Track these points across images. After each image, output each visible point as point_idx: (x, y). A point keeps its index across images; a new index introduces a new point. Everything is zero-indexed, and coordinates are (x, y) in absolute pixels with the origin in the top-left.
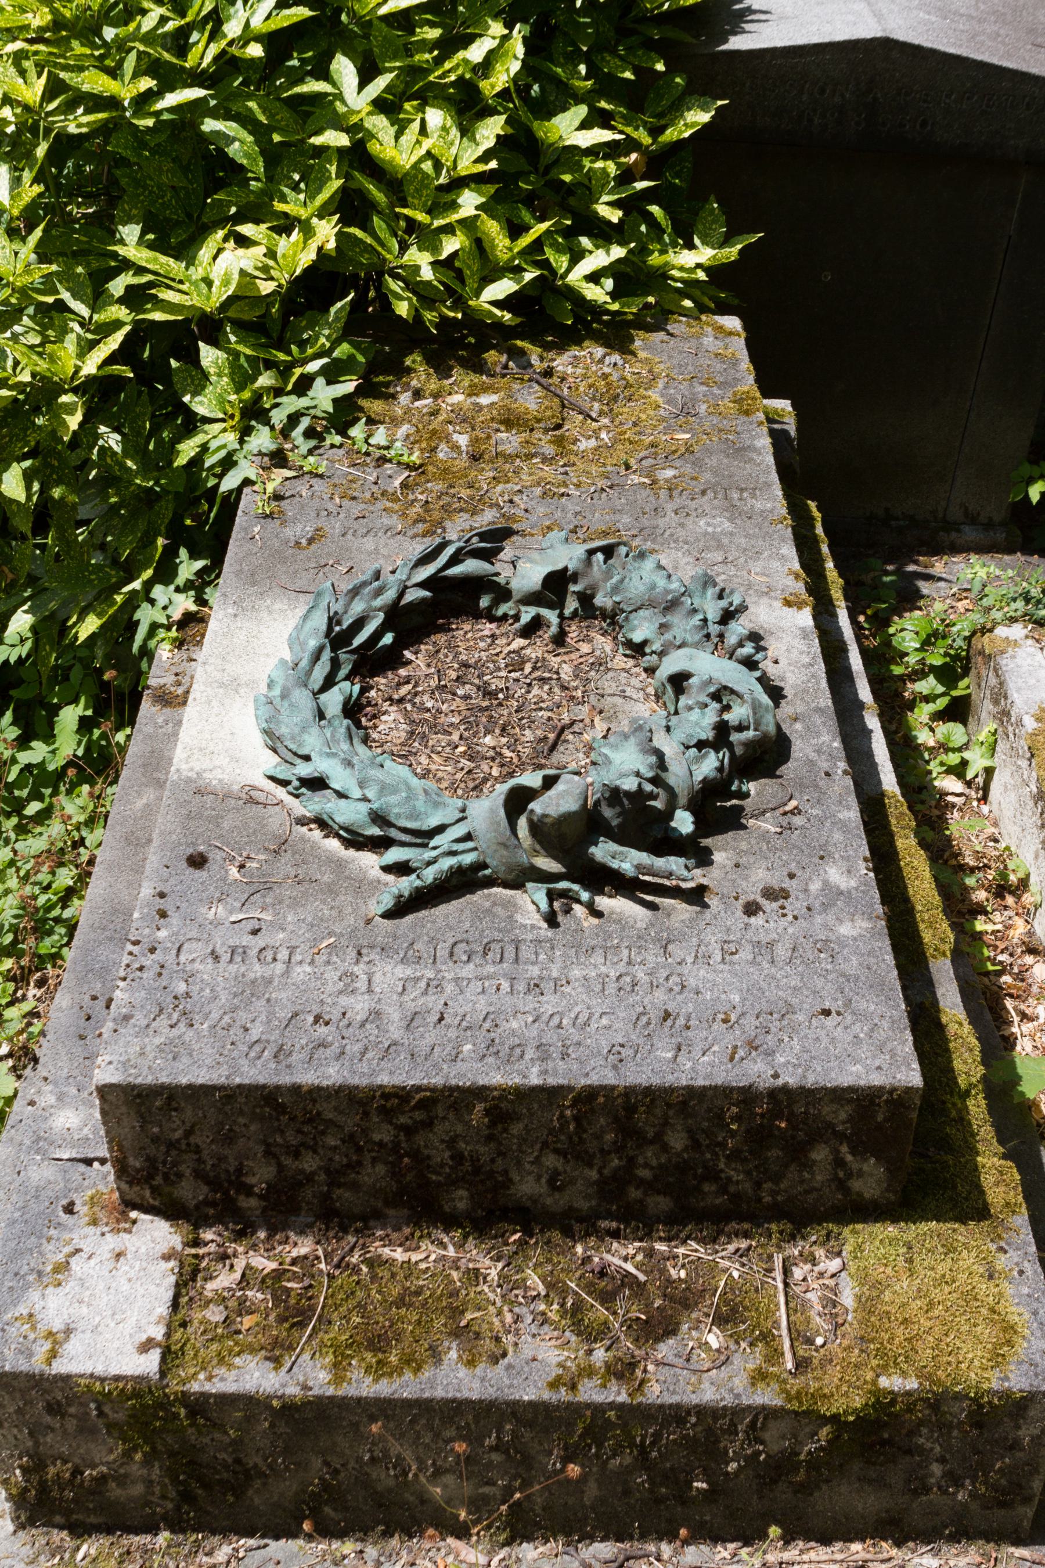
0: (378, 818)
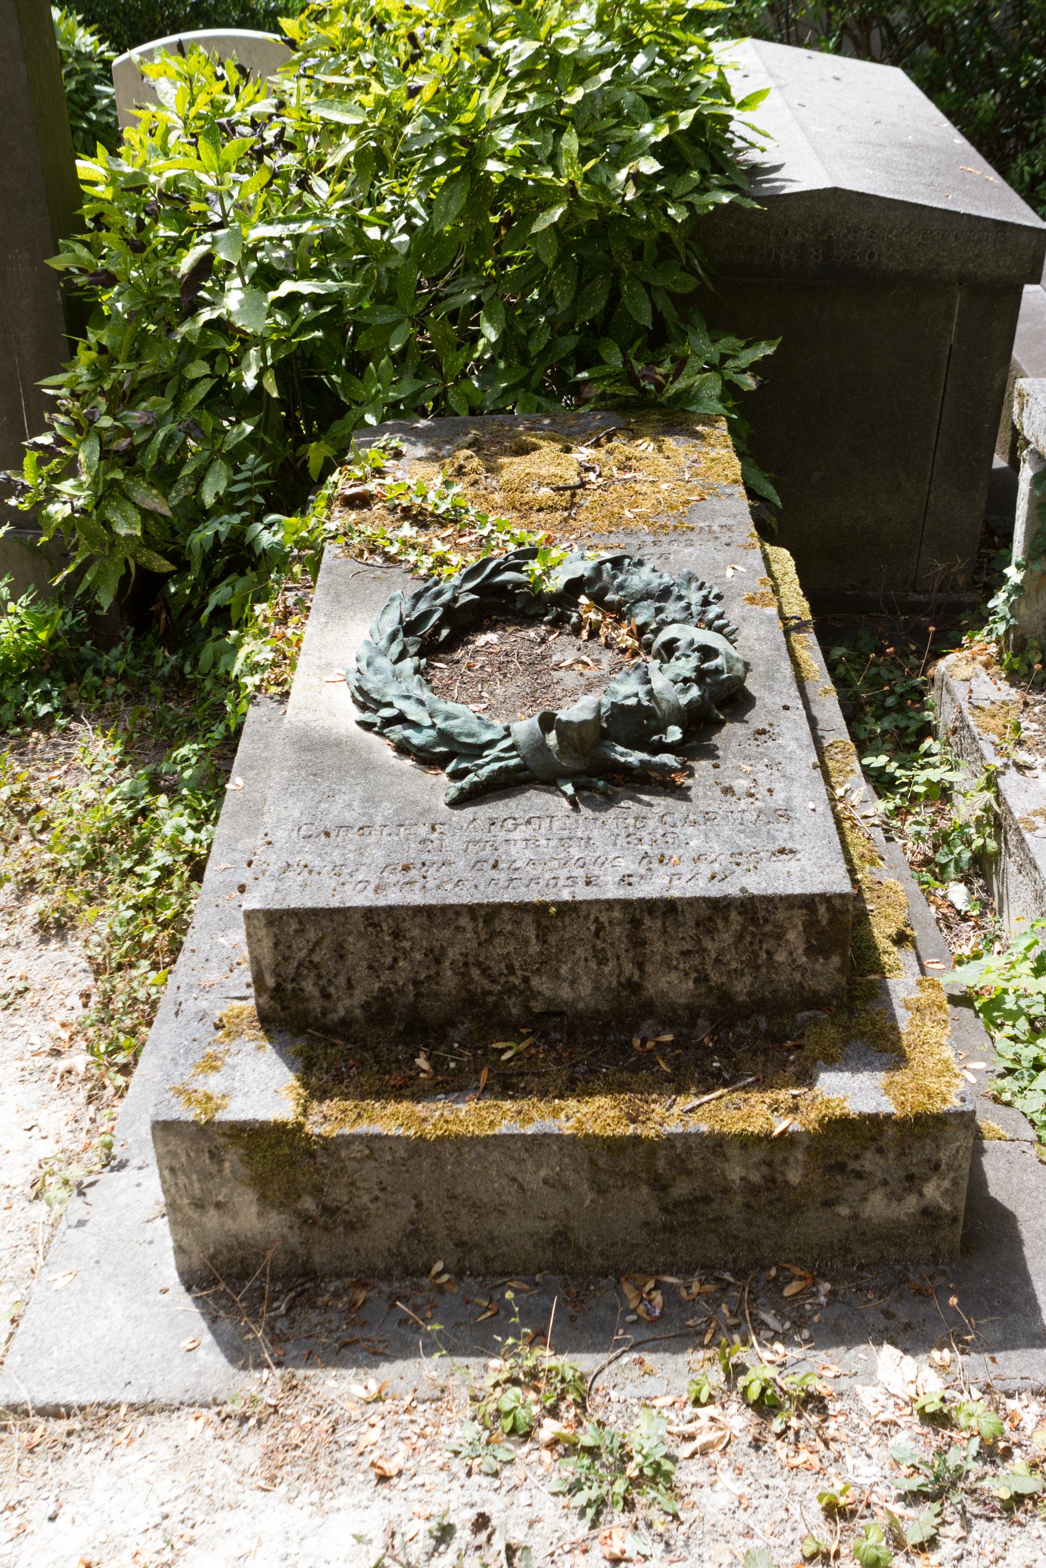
0: (445, 736)
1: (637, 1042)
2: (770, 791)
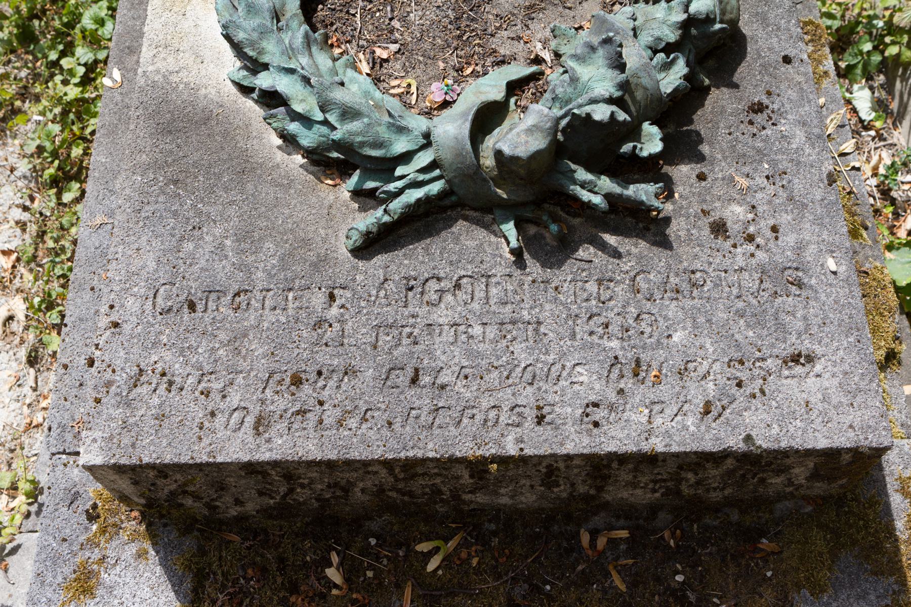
1: (585, 538)
2: (774, 229)
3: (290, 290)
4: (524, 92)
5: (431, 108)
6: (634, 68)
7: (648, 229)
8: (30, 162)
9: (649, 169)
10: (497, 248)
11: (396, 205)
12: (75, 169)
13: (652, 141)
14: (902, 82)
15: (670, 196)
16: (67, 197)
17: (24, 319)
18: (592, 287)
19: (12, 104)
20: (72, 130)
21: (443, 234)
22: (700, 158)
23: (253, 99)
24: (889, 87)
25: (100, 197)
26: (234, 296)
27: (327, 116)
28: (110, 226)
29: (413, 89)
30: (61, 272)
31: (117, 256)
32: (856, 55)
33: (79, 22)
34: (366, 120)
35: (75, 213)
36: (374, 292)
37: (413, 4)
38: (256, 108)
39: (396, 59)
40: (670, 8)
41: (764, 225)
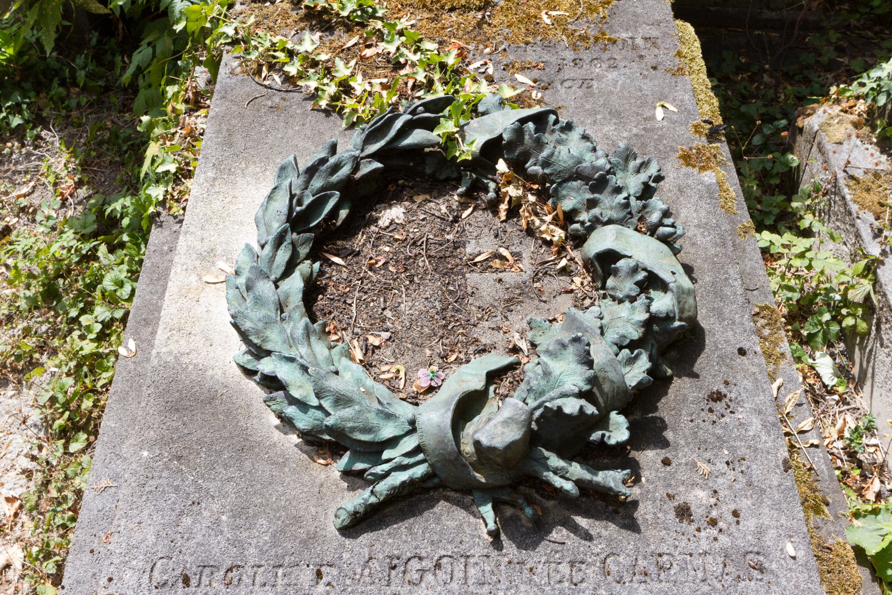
2: (735, 514)
3: (280, 566)
4: (502, 380)
5: (418, 393)
6: (601, 363)
7: (617, 513)
8: (42, 413)
9: (618, 456)
10: (476, 529)
11: (383, 487)
12: (84, 420)
13: (618, 431)
14: (860, 350)
15: (637, 480)
16: (74, 447)
17: (20, 568)
18: (565, 569)
19: (31, 357)
20: (84, 382)
21: (426, 514)
22: (664, 444)
23: (255, 381)
24: (849, 354)
25: (107, 461)
26: (227, 572)
27: (322, 402)
28: (113, 490)
29: (402, 375)
30: (61, 522)
31: (119, 529)
32: (816, 325)
33: (100, 283)
34: (357, 407)
35: (80, 464)
36: (359, 571)
37: (404, 296)
38: (258, 389)
39: (387, 346)
40: (633, 308)
41: (726, 509)
